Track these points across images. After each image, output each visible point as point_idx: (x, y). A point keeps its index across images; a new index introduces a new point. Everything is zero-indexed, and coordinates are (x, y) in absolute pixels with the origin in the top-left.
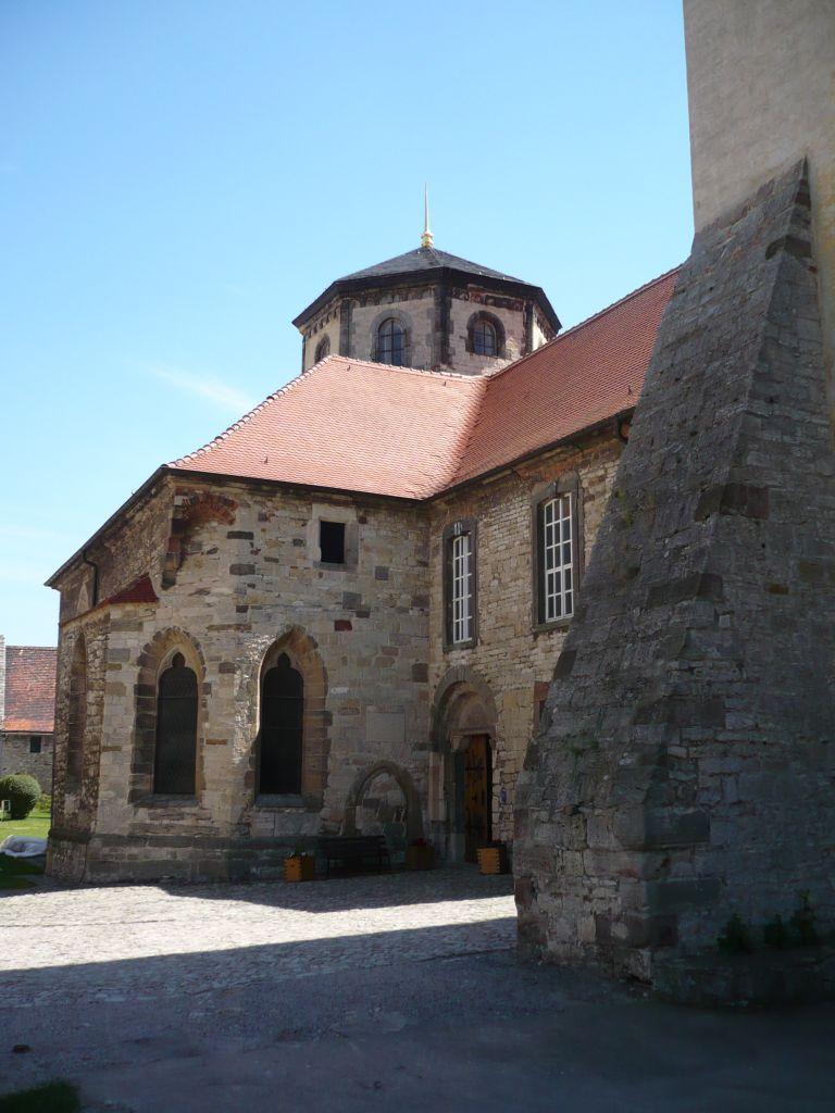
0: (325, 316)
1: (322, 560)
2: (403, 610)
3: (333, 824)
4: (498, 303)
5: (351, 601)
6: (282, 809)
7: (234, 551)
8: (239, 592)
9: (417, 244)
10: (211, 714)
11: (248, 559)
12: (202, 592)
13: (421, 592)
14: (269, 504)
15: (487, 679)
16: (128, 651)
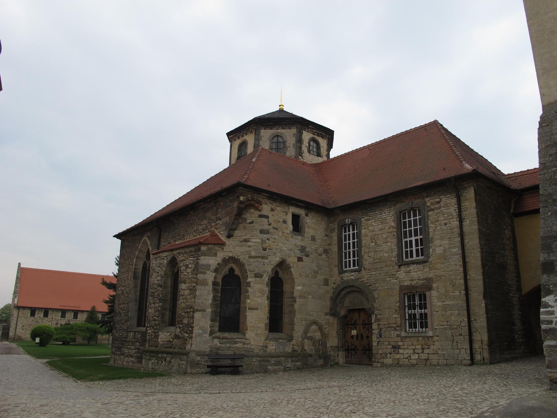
0: (245, 132)
1: (293, 230)
2: (320, 255)
3: (297, 347)
4: (318, 135)
5: (303, 249)
8: (263, 241)
9: (277, 109)
11: (266, 227)
12: (246, 241)
13: (326, 247)
14: (274, 204)
15: (368, 284)
16: (210, 265)
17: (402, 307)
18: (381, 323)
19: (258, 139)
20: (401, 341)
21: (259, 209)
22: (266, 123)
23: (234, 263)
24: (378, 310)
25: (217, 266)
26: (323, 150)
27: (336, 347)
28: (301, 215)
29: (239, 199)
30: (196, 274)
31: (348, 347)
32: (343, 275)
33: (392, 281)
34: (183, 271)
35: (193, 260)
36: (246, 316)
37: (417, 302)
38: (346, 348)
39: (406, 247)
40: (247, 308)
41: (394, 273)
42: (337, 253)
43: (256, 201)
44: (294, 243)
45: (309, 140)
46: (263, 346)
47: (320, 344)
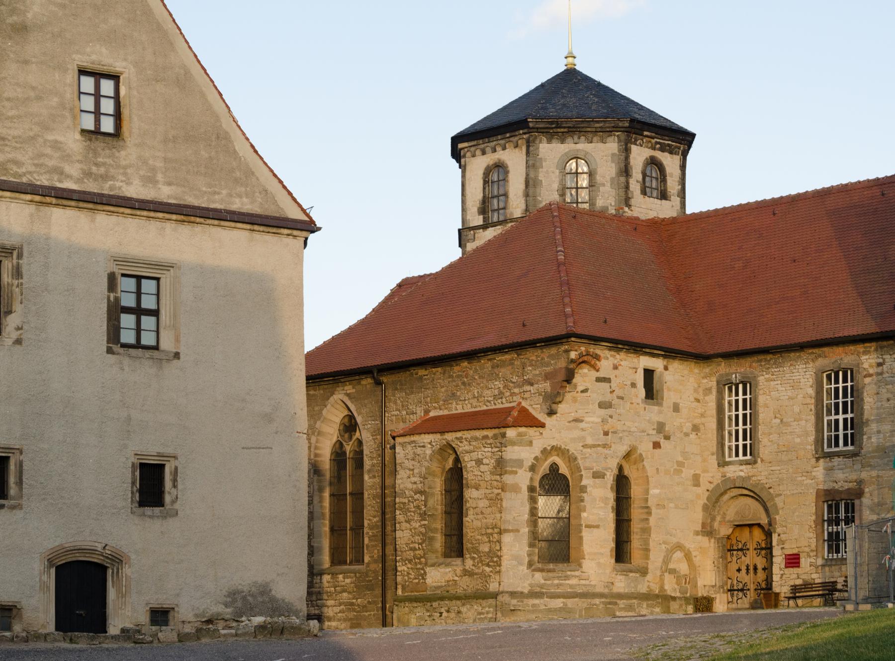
0: (502, 142)
2: (687, 435)
4: (662, 149)
6: (628, 573)
7: (600, 392)
10: (588, 507)
11: (608, 397)
12: (576, 420)
13: (697, 421)
14: (618, 356)
15: (767, 486)
17: (819, 521)
18: (786, 546)
19: (532, 164)
20: (816, 573)
21: (597, 368)
22: (552, 128)
23: (558, 455)
24: (783, 526)
25: (533, 461)
26: (672, 185)
27: (713, 586)
28: (658, 369)
29: (569, 355)
30: (501, 475)
31: (732, 585)
32: (726, 468)
33: (805, 482)
34: (472, 469)
35: (493, 453)
36: (581, 538)
37: (842, 515)
38: (729, 588)
39: (830, 430)
40: (584, 525)
41: (809, 469)
42: (715, 432)
43: (592, 356)
44: (648, 418)
45: (644, 164)
46: (608, 582)
47: (688, 581)
